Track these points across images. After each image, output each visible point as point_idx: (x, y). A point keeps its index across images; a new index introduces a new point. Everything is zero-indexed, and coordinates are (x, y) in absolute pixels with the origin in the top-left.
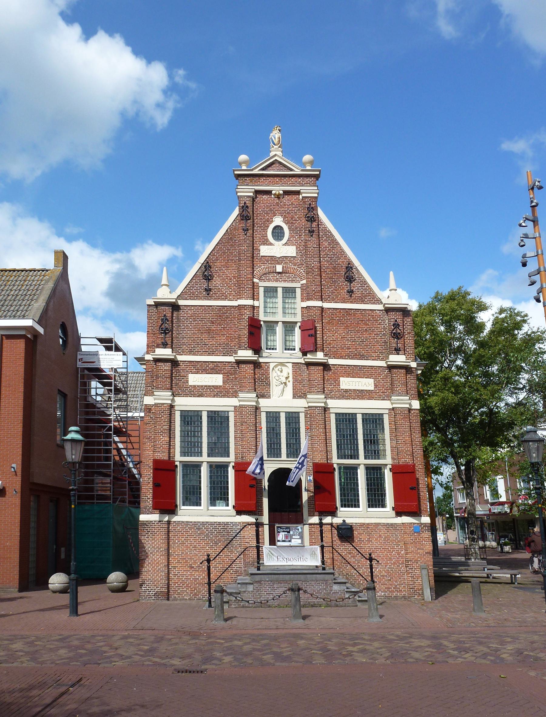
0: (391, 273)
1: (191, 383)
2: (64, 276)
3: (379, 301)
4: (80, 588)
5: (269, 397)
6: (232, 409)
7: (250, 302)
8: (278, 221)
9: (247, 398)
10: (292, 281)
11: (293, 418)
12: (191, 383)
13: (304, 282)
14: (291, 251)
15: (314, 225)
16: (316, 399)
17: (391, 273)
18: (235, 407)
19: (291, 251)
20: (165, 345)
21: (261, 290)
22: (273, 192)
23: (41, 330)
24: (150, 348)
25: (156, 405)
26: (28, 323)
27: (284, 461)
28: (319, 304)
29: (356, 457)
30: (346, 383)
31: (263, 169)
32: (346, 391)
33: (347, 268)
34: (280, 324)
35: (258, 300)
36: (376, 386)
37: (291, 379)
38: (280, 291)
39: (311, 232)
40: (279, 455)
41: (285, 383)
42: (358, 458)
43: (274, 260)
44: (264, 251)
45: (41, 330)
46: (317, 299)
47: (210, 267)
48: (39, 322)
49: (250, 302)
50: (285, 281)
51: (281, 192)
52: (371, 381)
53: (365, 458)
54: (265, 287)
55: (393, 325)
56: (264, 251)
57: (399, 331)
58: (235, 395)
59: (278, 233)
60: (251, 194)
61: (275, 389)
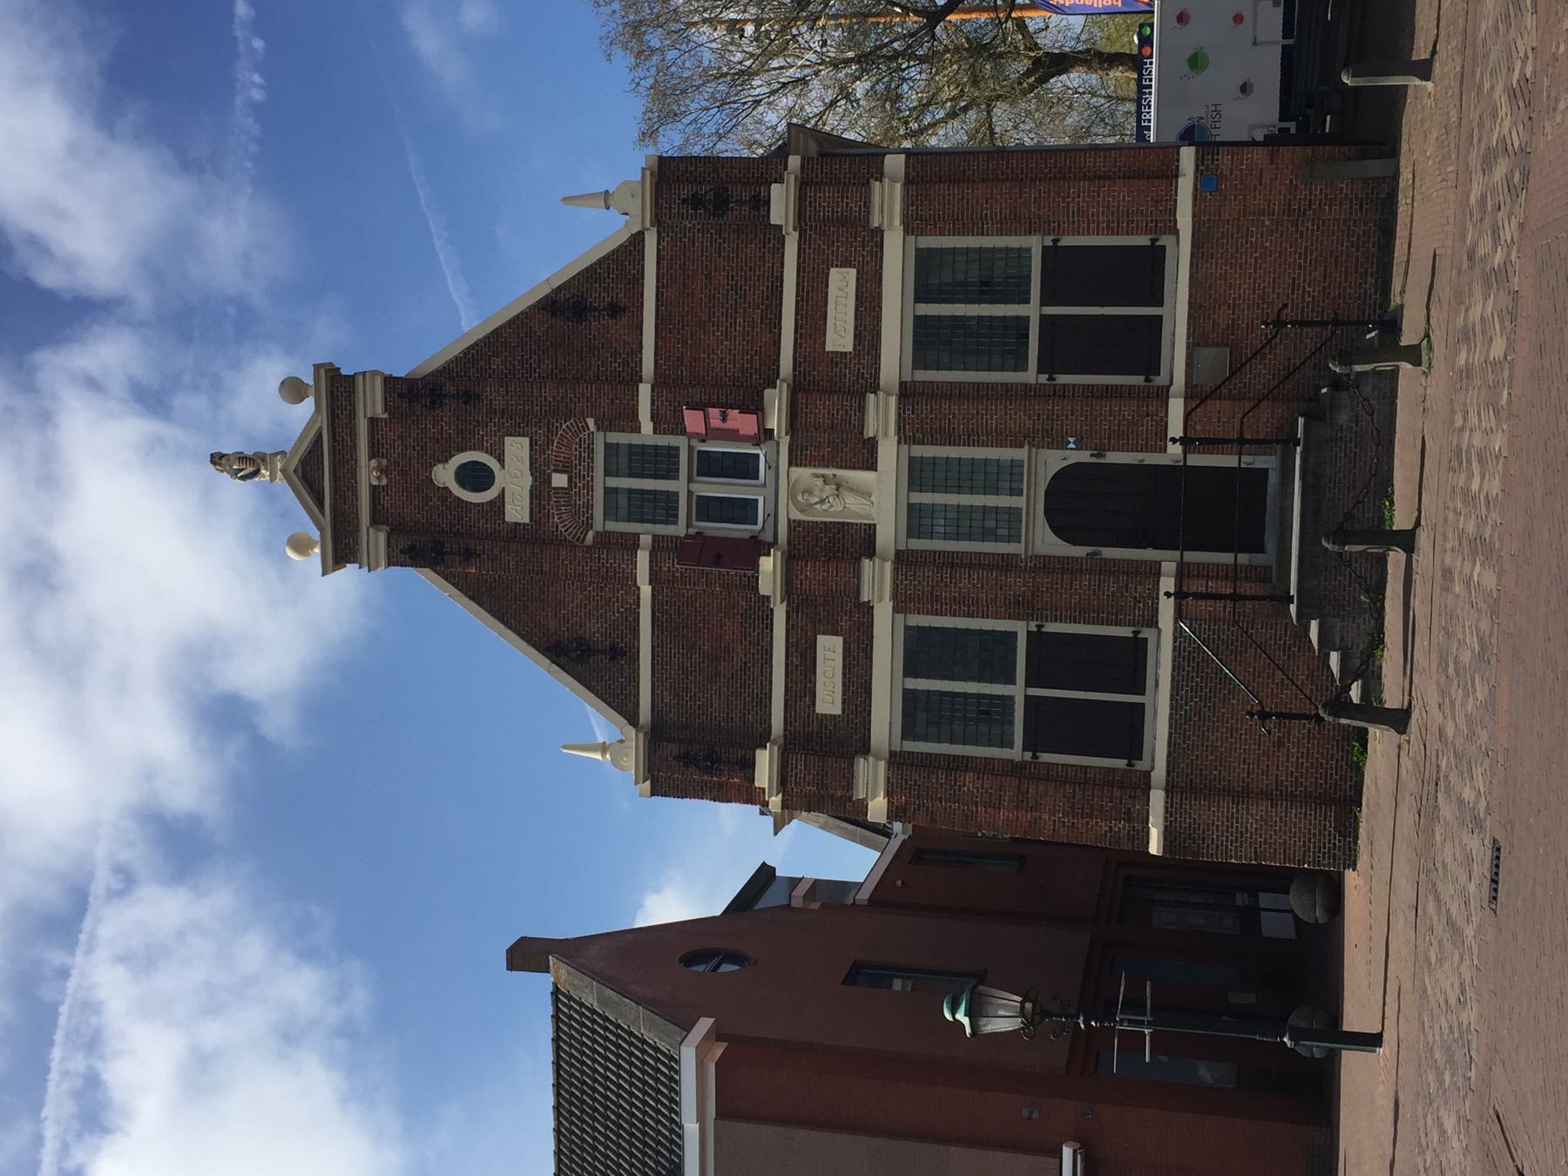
0: (1154, 848)
1: (836, 710)
2: (573, 950)
3: (637, 240)
4: (1346, 1028)
5: (872, 527)
6: (900, 617)
7: (643, 559)
8: (445, 475)
9: (876, 581)
10: (591, 451)
11: (919, 475)
12: (836, 710)
13: (591, 422)
14: (517, 448)
15: (450, 388)
16: (881, 417)
17: (1154, 848)
18: (896, 610)
19: (517, 448)
20: (749, 766)
21: (613, 526)
22: (375, 483)
23: (704, 1025)
24: (750, 795)
25: (889, 794)
26: (688, 1057)
27: (1031, 503)
28: (645, 391)
29: (1023, 322)
30: (840, 336)
31: (323, 514)
32: (858, 337)
33: (554, 314)
34: (693, 487)
35: (636, 536)
36: (846, 264)
37: (829, 472)
38: (614, 482)
39: (469, 397)
40: (1014, 513)
41: (838, 486)
42: (1027, 319)
43: (540, 492)
44: (518, 511)
45: (704, 1025)
46: (635, 395)
47: (558, 644)
48: (687, 1027)
49: (643, 559)
50: (590, 469)
51: (374, 463)
52: (835, 274)
53: (1027, 301)
54: (606, 517)
55: (695, 208)
56: (518, 511)
57: (710, 196)
58: (868, 609)
59: (476, 477)
60: (382, 537)
61: (850, 509)
